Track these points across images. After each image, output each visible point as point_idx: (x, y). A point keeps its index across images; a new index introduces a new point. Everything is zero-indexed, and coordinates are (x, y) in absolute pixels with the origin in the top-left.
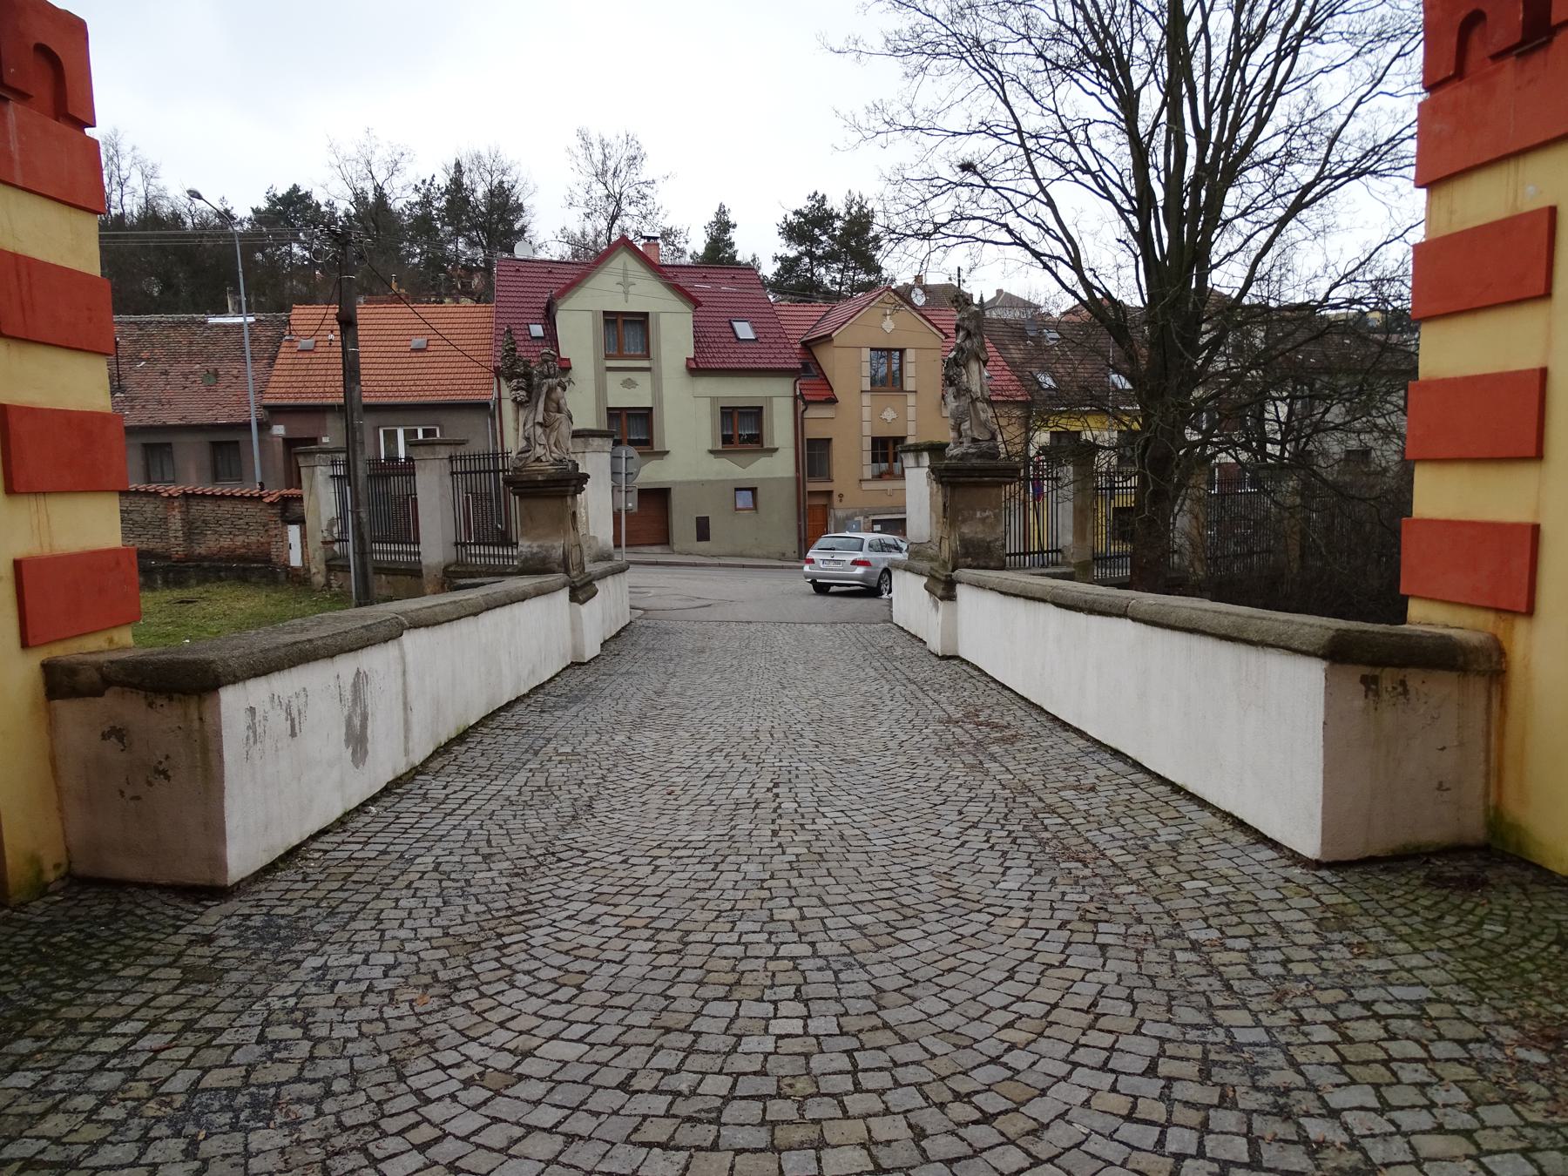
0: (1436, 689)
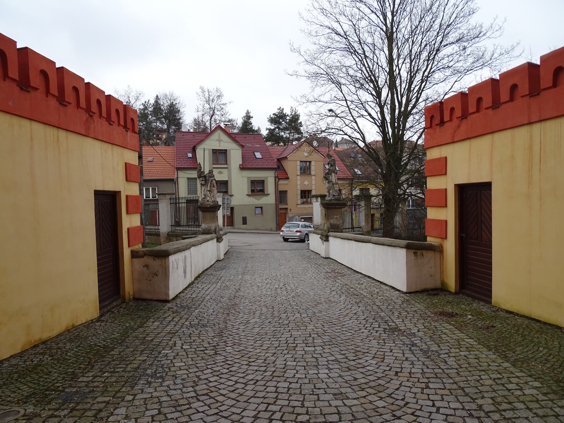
0: (429, 255)
